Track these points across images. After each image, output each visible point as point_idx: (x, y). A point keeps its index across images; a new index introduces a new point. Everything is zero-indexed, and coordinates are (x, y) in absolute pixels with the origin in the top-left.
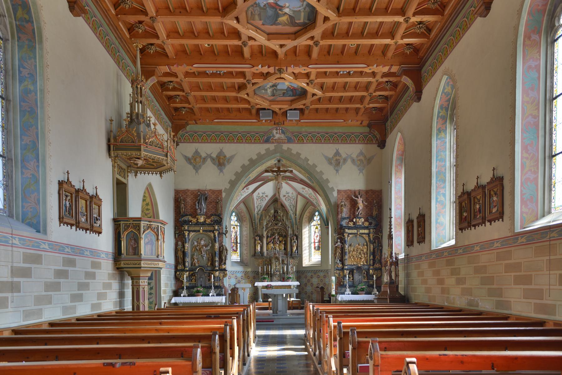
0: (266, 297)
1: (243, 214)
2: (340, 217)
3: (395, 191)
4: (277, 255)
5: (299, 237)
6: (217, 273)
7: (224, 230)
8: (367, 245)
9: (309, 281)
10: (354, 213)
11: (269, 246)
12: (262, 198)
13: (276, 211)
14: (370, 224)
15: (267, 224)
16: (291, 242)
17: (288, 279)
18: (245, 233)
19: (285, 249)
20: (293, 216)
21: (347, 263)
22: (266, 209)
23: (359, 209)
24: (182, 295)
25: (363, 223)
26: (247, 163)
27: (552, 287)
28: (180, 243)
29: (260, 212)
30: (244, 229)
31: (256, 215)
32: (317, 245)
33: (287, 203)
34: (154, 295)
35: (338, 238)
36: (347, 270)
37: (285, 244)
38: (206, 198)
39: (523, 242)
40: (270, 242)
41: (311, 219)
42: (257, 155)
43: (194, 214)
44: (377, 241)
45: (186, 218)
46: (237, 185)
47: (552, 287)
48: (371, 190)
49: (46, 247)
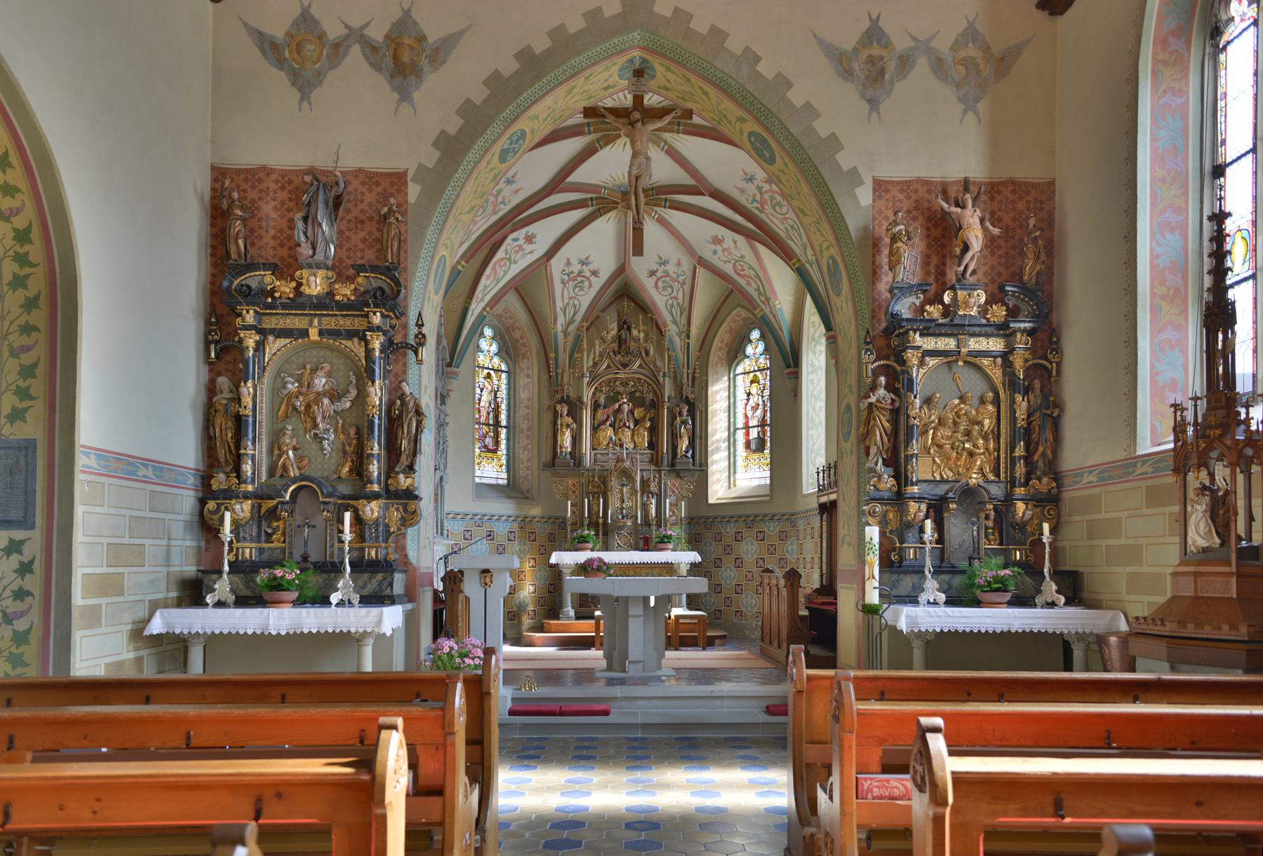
0: (585, 604)
1: (517, 335)
2: (883, 286)
3: (1154, 150)
4: (627, 464)
5: (700, 405)
6: (372, 510)
7: (413, 330)
8: (996, 402)
9: (728, 549)
10: (941, 274)
11: (601, 434)
12: (577, 279)
13: (624, 325)
14: (1013, 313)
15: (595, 364)
16: (672, 425)
17: (662, 543)
18: (523, 395)
19: (653, 445)
20: (677, 340)
21: (922, 469)
22: (593, 320)
23: (966, 248)
24: (209, 599)
25: (984, 311)
26: (509, 66)
27: (173, 543)
28: (223, 381)
30: (522, 381)
31: (561, 336)
32: (754, 433)
33: (660, 300)
34: (35, 603)
35: (876, 373)
36: (920, 499)
37: (654, 431)
38: (337, 202)
39: (1146, 473)
40: (604, 422)
41: (735, 353)
42: (551, 34)
43: (286, 267)
44: (1037, 384)
45: (253, 279)
46: (471, 156)
47: (173, 543)
48: (1013, 182)
49: (150, 473)
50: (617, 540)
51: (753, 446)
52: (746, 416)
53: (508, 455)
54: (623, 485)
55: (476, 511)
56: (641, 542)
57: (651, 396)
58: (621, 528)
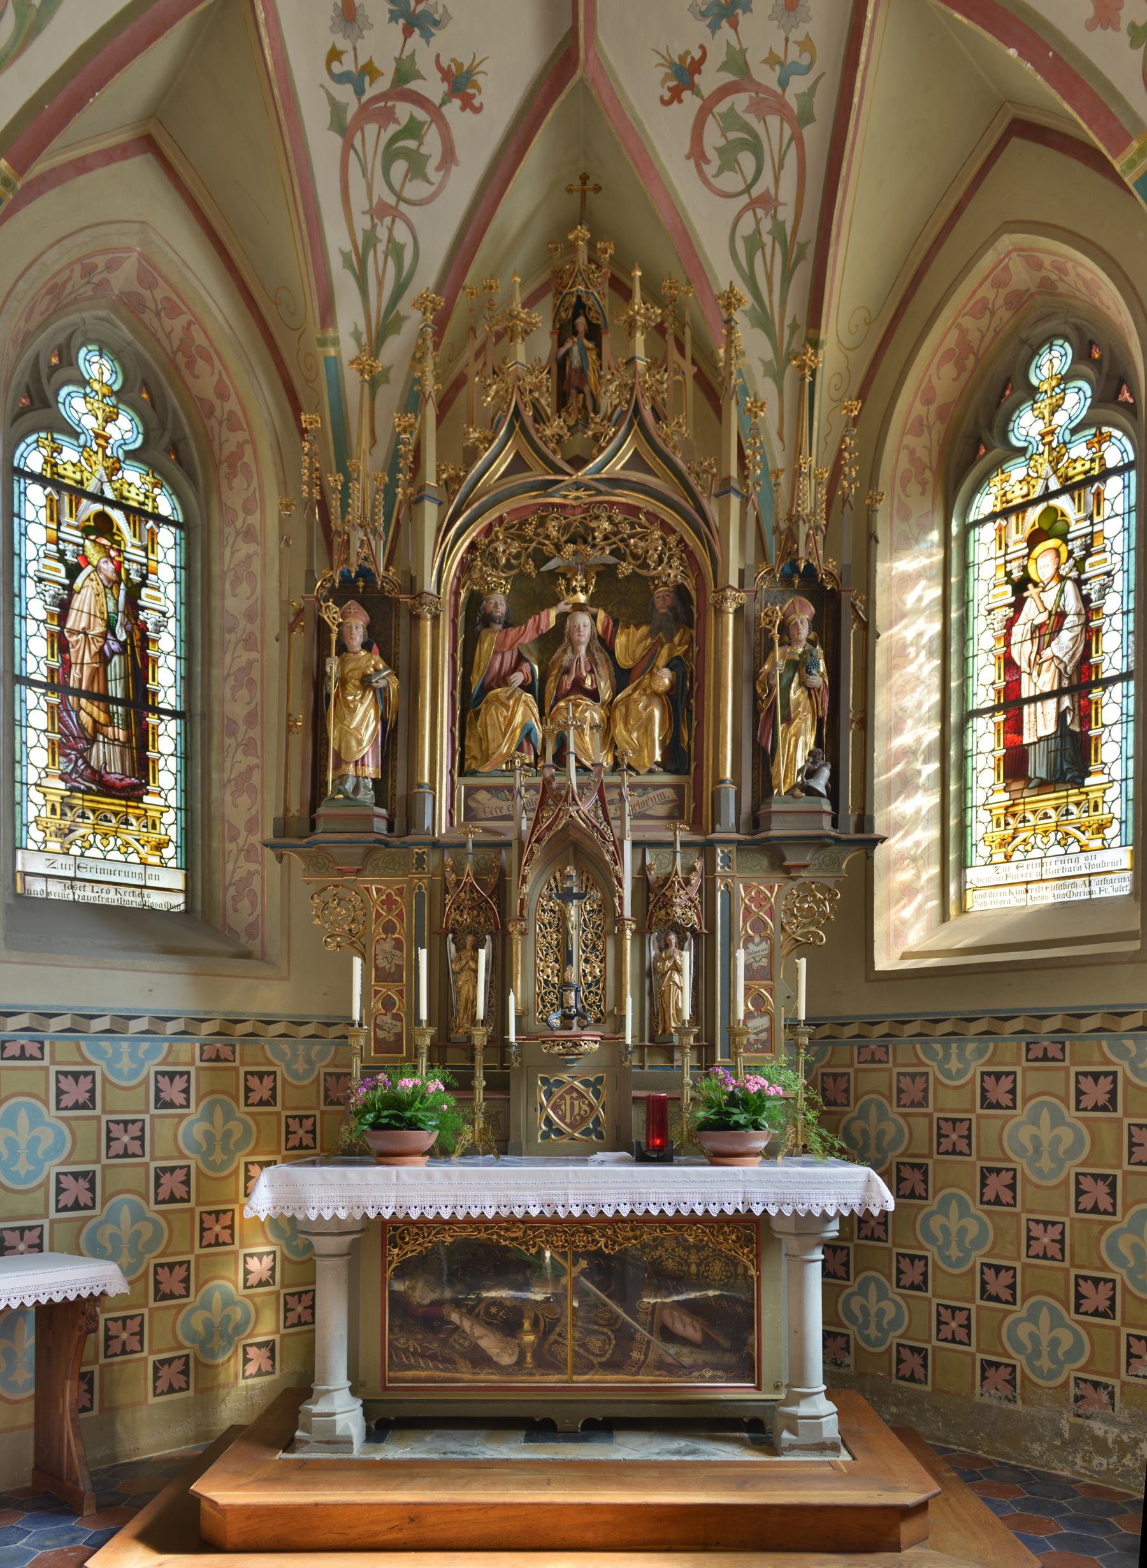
11: (492, 716)
17: (723, 1129)
19: (679, 757)
29: (395, 348)
32: (1040, 722)
37: (685, 704)
40: (502, 680)
41: (972, 444)
50: (541, 1107)
51: (1038, 767)
52: (1009, 665)
53: (187, 809)
54: (567, 896)
55: (90, 1004)
56: (638, 1117)
57: (674, 573)
58: (560, 1063)
